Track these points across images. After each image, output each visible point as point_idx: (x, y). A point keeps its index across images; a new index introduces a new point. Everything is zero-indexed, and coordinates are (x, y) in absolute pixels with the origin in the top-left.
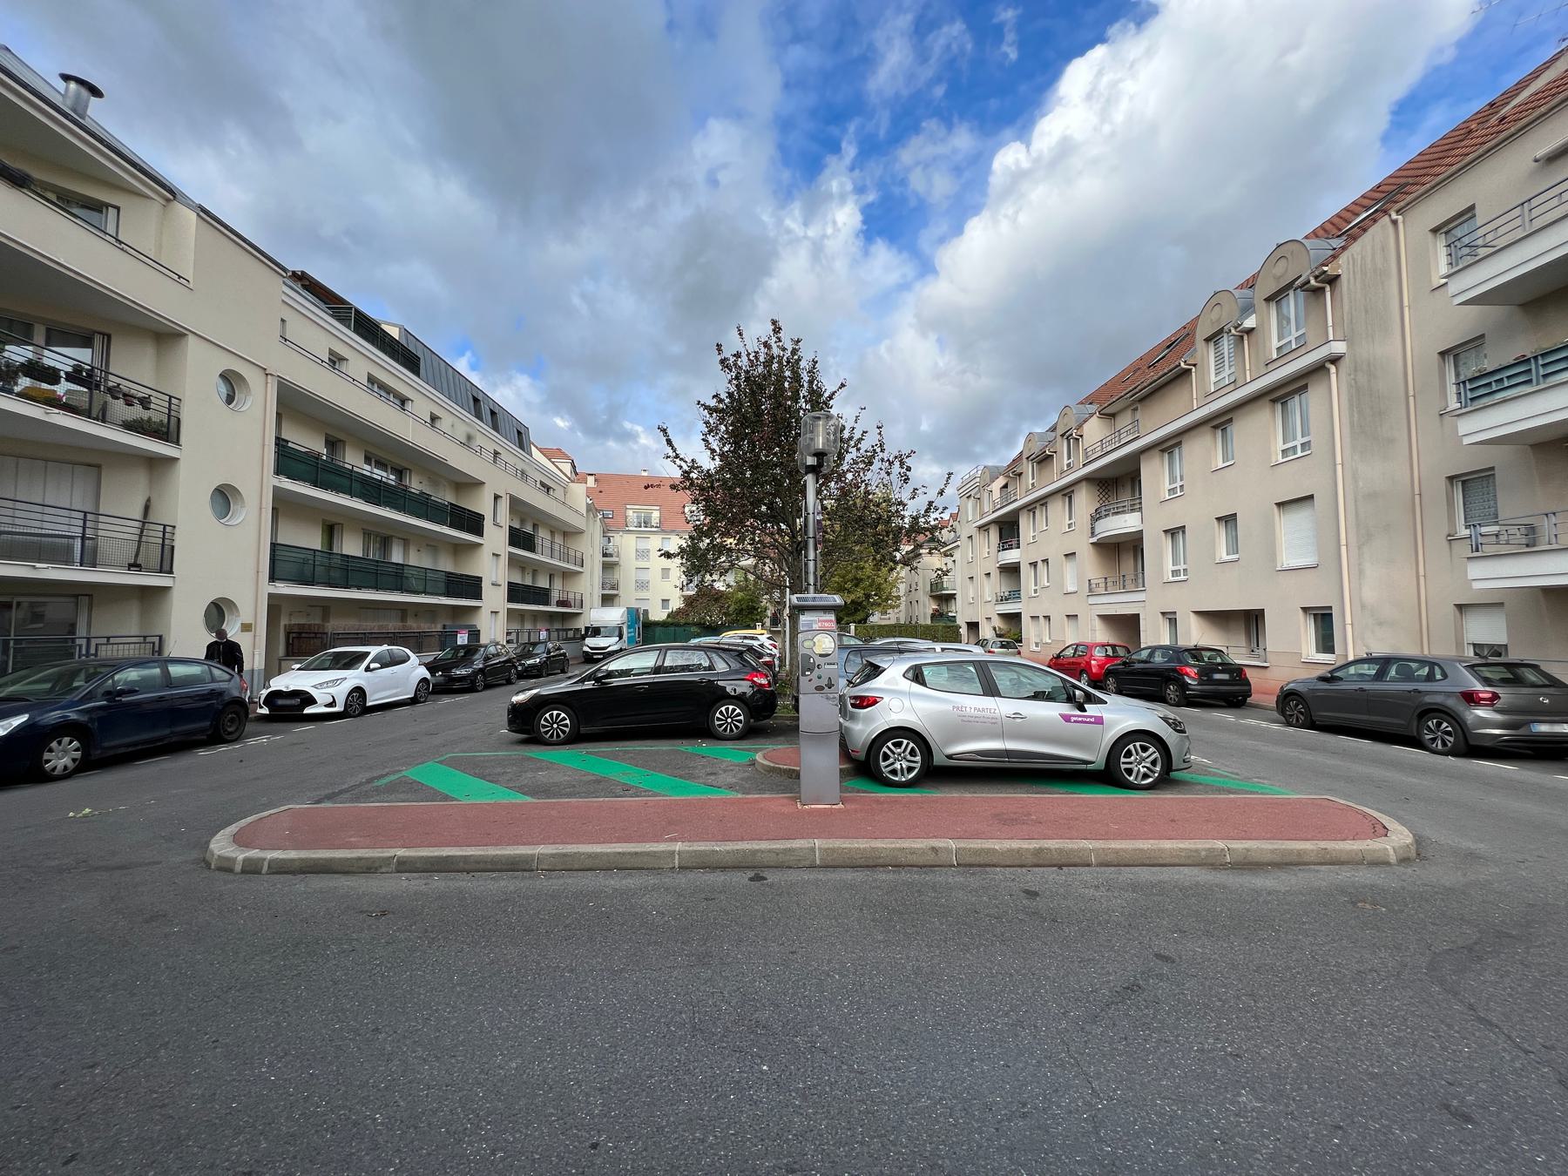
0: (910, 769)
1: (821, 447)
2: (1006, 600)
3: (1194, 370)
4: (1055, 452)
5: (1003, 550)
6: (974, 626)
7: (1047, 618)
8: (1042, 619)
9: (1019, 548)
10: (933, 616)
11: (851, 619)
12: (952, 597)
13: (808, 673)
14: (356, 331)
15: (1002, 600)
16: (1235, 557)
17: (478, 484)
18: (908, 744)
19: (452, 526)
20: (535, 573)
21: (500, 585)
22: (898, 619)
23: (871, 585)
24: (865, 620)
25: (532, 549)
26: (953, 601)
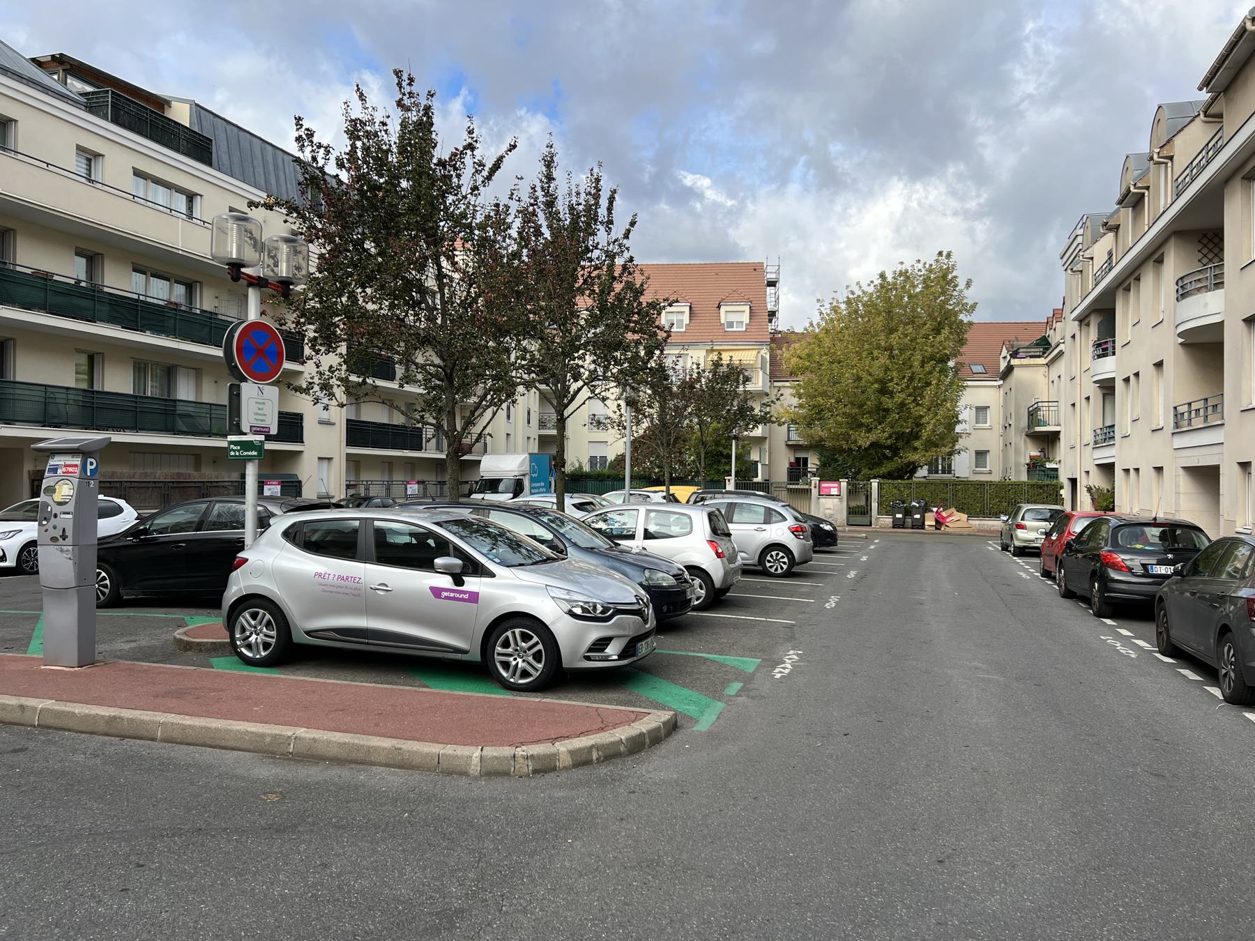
0: (525, 674)
1: (234, 256)
3: (1146, 194)
4: (1148, 188)
8: (1132, 472)
9: (1114, 354)
13: (44, 523)
14: (115, 121)
18: (537, 643)
21: (333, 424)
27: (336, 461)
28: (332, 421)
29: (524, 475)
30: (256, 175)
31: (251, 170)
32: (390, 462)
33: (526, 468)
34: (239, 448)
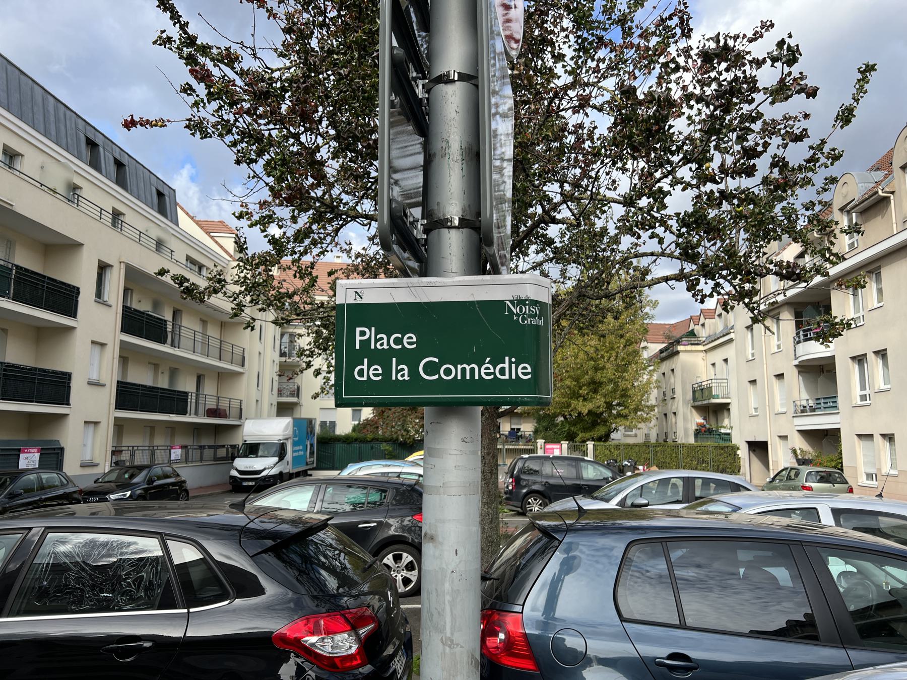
2: (813, 409)
3: (892, 197)
4: (893, 193)
5: (805, 340)
6: (759, 448)
7: (889, 438)
8: (878, 439)
10: (697, 433)
11: (588, 435)
12: (725, 407)
15: (802, 411)
16: (888, 387)
17: (74, 246)
19: (17, 298)
20: (173, 373)
21: (103, 385)
22: (647, 436)
23: (614, 391)
24: (606, 437)
25: (162, 340)
26: (726, 414)
27: (103, 427)
28: (102, 382)
29: (287, 439)
30: (36, 122)
31: (31, 115)
32: (152, 426)
33: (289, 432)
34: (410, 340)
